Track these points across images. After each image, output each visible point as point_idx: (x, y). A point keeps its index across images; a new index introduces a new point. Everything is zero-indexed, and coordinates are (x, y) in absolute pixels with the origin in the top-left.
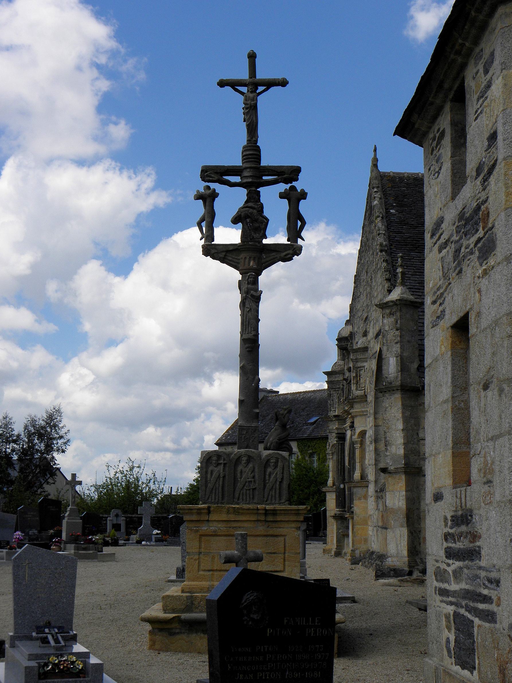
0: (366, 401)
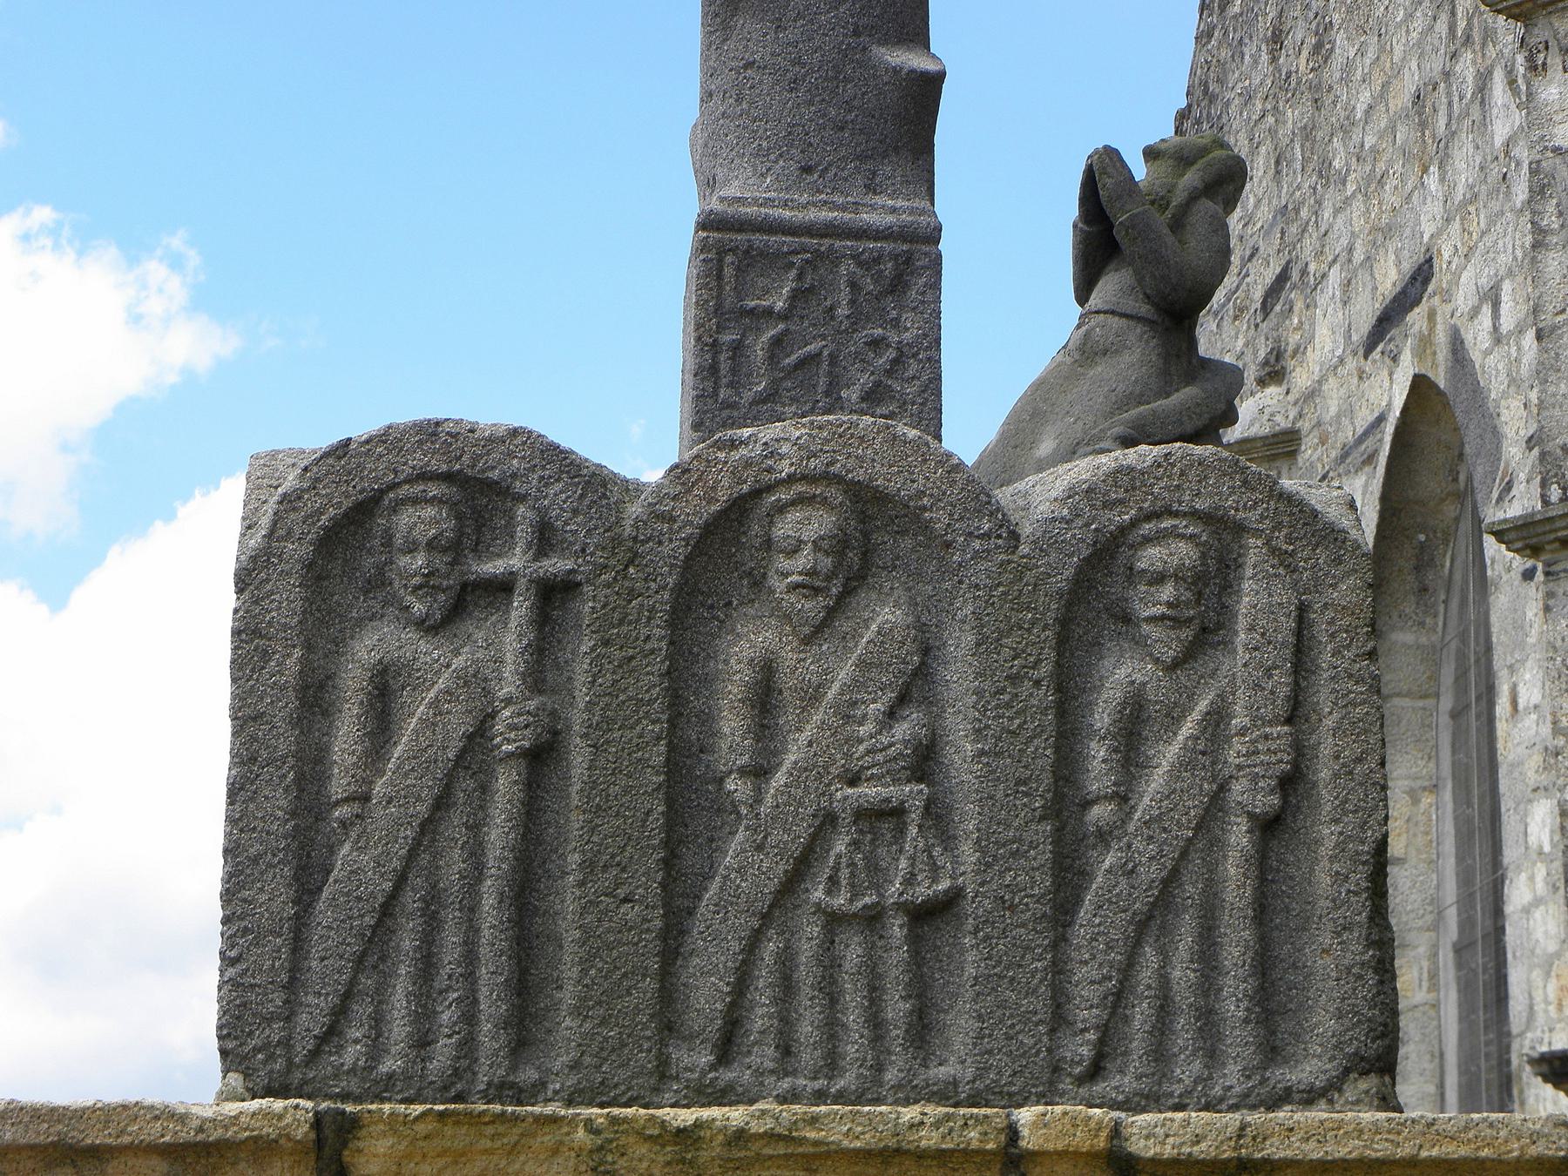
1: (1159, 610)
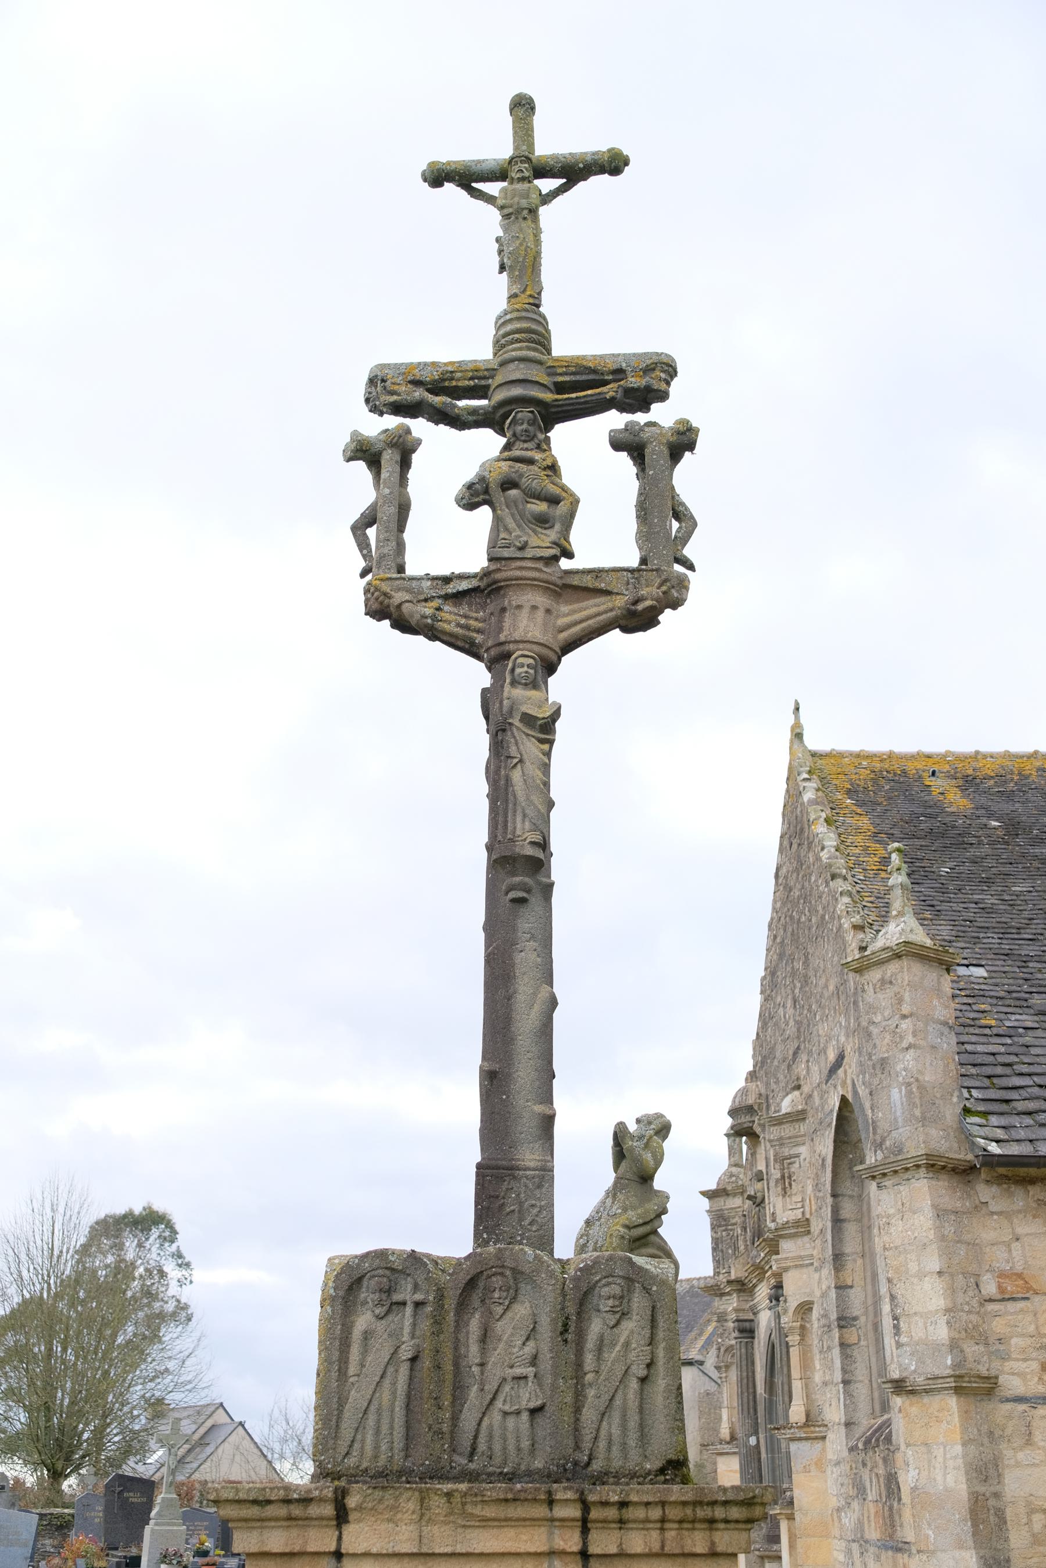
0: (809, 1232)
1: (608, 1309)
